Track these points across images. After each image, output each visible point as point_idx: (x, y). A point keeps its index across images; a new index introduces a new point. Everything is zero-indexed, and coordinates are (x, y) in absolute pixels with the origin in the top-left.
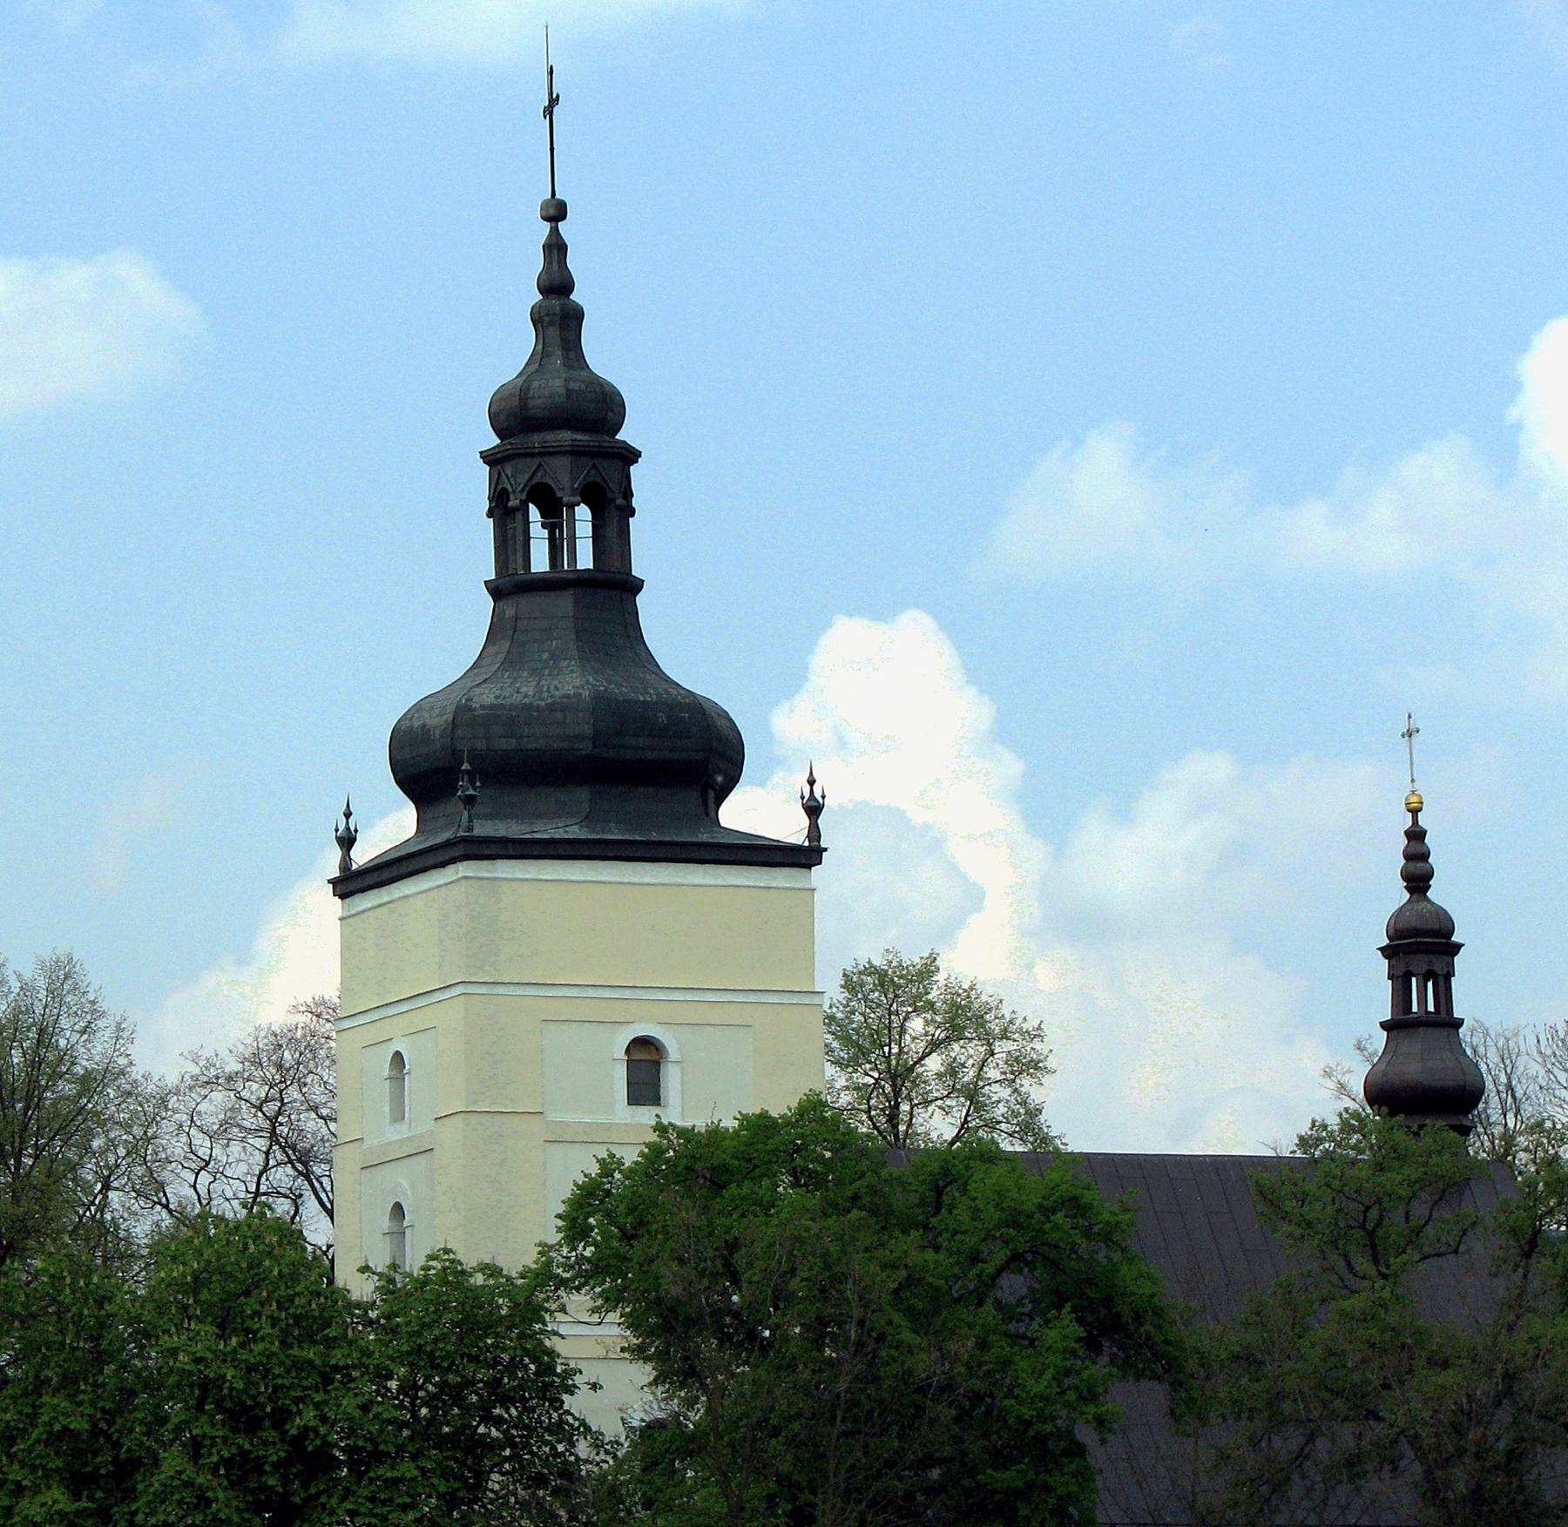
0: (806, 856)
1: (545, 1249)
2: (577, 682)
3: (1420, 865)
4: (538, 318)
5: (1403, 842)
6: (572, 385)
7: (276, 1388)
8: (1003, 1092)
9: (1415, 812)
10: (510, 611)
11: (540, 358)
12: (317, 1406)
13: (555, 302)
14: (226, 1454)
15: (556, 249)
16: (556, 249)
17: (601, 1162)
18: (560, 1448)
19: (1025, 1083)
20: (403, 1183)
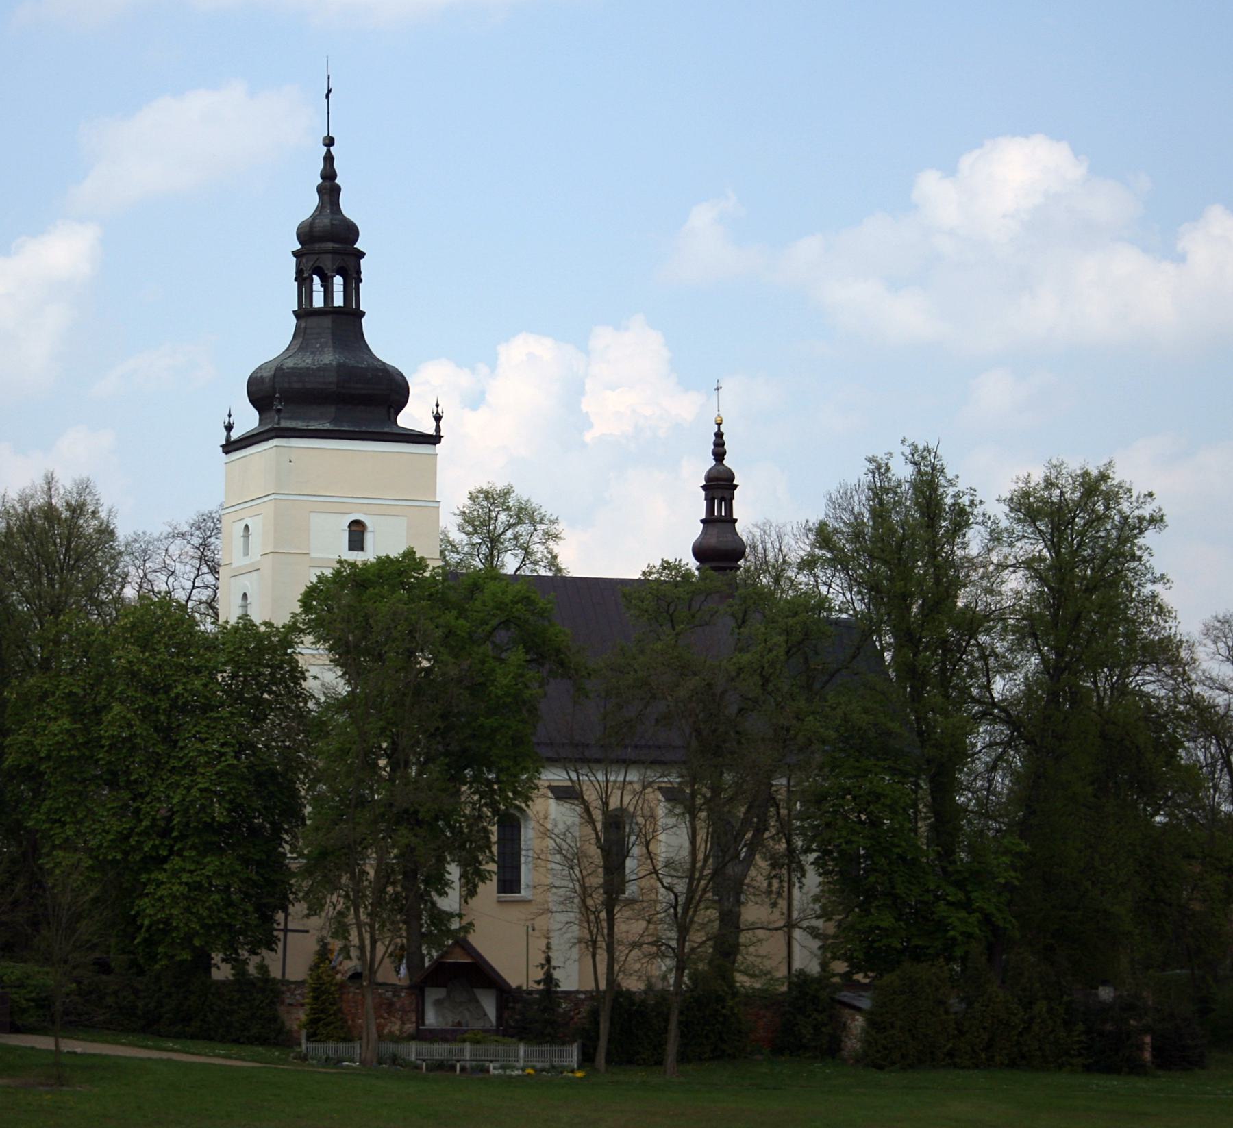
0: (434, 439)
1: (294, 615)
2: (331, 358)
3: (720, 449)
4: (320, 190)
5: (713, 438)
6: (334, 222)
7: (166, 675)
8: (541, 548)
9: (719, 424)
10: (303, 325)
11: (320, 209)
12: (184, 684)
13: (327, 184)
14: (141, 704)
15: (329, 159)
16: (329, 159)
17: (319, 577)
18: (301, 705)
19: (551, 544)
20: (248, 583)
